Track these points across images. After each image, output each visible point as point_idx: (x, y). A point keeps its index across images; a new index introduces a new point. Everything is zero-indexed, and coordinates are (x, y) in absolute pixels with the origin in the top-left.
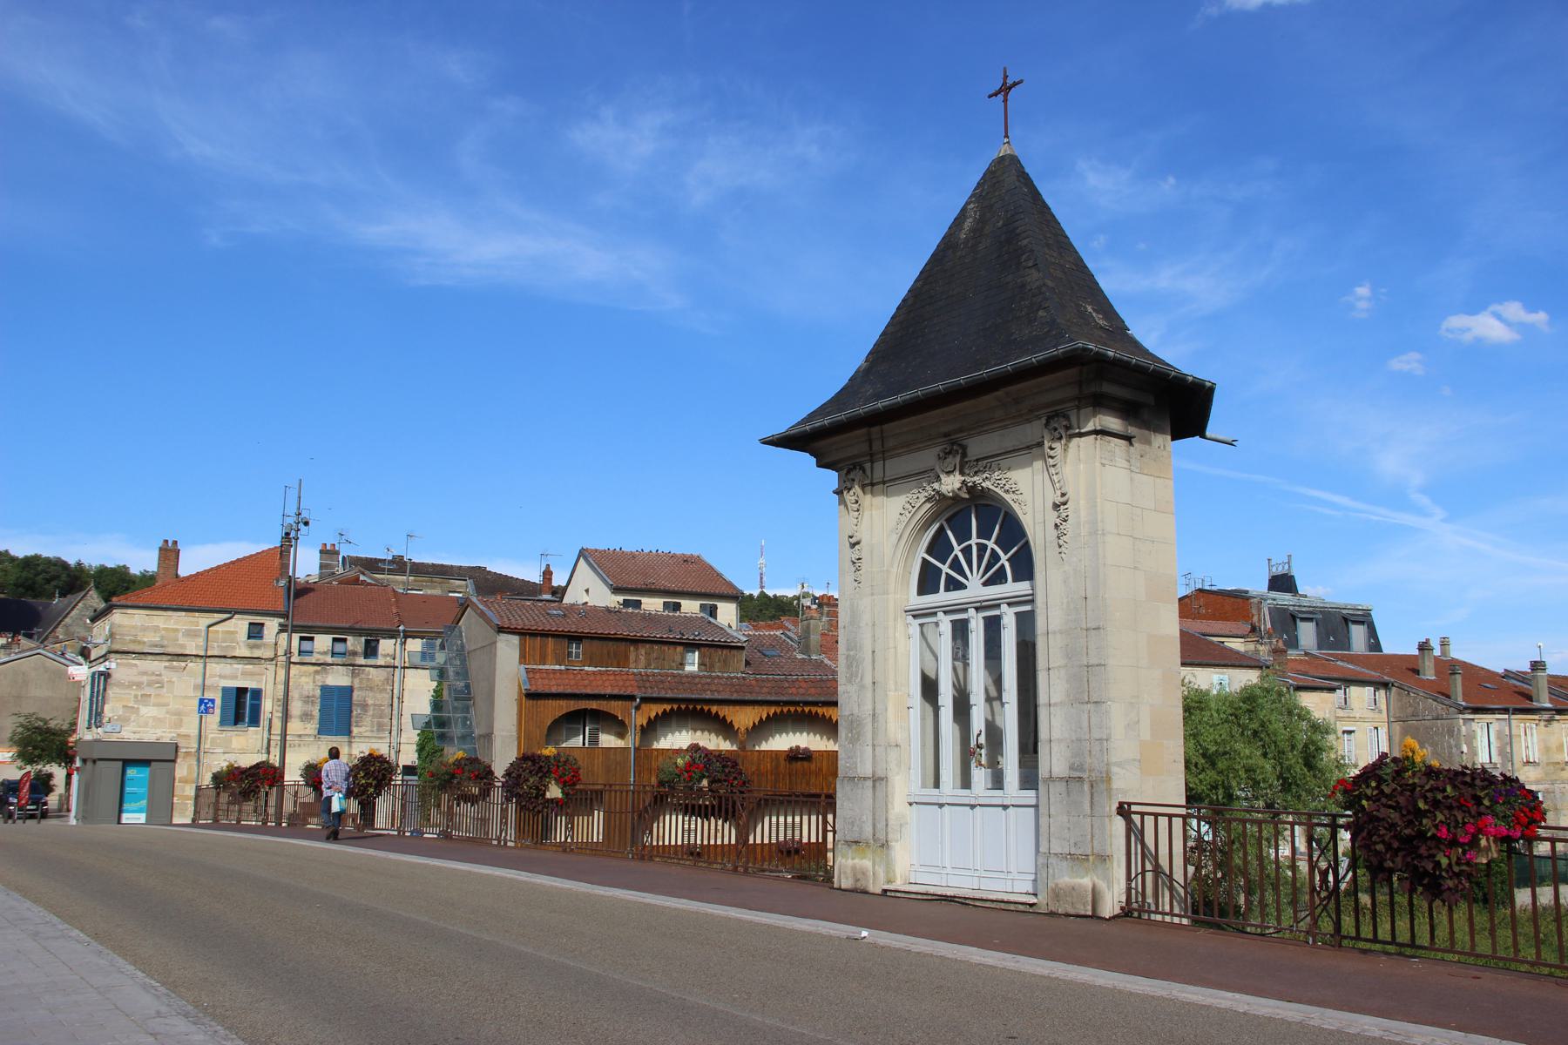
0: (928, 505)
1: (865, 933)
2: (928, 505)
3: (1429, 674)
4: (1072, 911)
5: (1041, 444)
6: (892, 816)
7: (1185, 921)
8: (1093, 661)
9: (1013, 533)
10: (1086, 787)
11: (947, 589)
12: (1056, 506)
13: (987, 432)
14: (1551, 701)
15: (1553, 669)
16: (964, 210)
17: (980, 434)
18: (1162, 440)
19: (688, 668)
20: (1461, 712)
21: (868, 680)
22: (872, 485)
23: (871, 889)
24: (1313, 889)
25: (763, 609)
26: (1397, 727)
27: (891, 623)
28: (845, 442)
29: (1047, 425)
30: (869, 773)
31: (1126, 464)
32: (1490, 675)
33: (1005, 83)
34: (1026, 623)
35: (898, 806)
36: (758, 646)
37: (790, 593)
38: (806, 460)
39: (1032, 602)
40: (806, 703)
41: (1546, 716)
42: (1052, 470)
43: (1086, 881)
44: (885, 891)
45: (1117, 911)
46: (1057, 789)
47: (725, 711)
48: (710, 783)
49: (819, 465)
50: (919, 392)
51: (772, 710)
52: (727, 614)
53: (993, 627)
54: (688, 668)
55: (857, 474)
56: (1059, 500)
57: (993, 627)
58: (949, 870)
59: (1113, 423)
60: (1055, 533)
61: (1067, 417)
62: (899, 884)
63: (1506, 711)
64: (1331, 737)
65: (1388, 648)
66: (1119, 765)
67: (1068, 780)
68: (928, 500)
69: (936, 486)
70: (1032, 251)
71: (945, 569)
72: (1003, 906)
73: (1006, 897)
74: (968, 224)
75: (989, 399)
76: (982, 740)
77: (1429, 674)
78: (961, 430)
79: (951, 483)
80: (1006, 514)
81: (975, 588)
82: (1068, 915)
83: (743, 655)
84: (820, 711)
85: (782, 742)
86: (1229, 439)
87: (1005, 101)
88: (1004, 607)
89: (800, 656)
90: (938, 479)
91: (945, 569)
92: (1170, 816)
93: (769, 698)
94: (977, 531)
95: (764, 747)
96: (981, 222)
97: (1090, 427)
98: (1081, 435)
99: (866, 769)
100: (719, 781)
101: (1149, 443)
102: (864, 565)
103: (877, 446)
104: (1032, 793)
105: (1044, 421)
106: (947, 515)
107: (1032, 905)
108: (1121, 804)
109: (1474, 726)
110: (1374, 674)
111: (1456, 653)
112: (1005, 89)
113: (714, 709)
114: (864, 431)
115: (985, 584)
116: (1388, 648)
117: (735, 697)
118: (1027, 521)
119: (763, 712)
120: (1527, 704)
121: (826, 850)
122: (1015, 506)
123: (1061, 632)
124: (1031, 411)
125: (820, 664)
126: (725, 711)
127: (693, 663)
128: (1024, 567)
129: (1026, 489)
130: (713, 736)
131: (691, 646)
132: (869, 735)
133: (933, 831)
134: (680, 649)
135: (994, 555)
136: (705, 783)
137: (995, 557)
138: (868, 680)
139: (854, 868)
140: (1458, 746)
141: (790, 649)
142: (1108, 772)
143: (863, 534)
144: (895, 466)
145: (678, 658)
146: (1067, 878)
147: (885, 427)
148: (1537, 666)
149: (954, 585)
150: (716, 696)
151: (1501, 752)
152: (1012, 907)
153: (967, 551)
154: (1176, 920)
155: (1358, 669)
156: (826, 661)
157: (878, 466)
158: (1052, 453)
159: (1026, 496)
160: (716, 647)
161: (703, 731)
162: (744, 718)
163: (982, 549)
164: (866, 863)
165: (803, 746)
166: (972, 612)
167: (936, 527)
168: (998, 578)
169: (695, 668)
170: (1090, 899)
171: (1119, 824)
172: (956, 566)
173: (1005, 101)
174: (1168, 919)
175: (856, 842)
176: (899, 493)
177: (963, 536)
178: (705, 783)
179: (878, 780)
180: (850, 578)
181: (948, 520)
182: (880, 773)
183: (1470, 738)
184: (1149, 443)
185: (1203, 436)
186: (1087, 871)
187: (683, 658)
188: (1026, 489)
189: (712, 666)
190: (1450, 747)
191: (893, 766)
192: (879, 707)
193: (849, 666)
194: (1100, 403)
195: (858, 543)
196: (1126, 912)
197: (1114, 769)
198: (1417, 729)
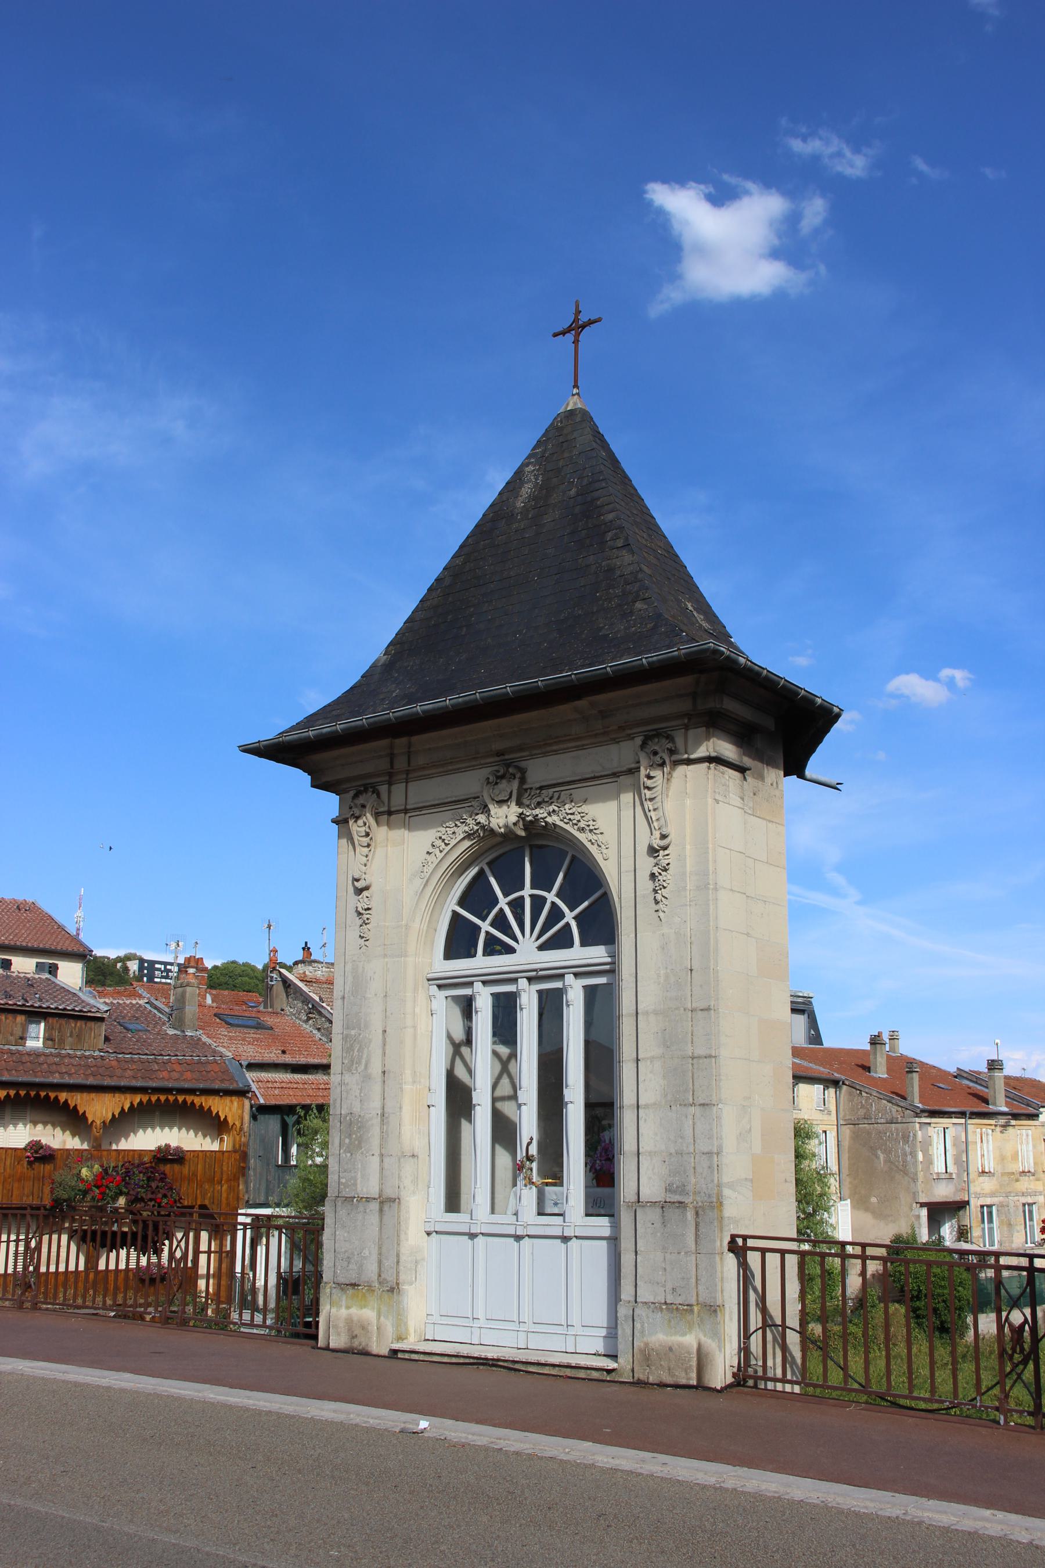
0: (467, 843)
1: (423, 1424)
2: (467, 843)
3: (881, 1072)
4: (669, 1380)
5: (634, 771)
6: (405, 1250)
7: (797, 1389)
8: (700, 1051)
9: (585, 882)
10: (690, 1215)
11: (489, 951)
12: (653, 851)
13: (556, 752)
14: (1007, 1104)
15: (1011, 1069)
16: (519, 474)
17: (545, 754)
18: (774, 775)
19: (31, 1044)
20: (917, 1115)
21: (376, 1069)
22: (390, 813)
23: (375, 1349)
24: (1002, 1352)
25: (102, 973)
26: (847, 1131)
27: (409, 994)
28: (354, 756)
29: (643, 746)
30: (374, 1192)
31: (737, 801)
32: (943, 1074)
33: (576, 320)
34: (601, 1003)
35: (413, 1236)
36: (117, 1016)
37: (113, 954)
38: (298, 778)
39: (612, 971)
40: (191, 1091)
41: (1002, 1121)
42: (649, 805)
43: (690, 1340)
44: (394, 1352)
45: (730, 1380)
46: (647, 1218)
47: (77, 1100)
48: (130, 1202)
49: (314, 785)
50: (477, 695)
51: (137, 1099)
52: (71, 974)
53: (551, 1006)
54: (31, 1044)
55: (368, 799)
56: (657, 843)
57: (551, 1006)
58: (482, 1323)
59: (727, 749)
60: (650, 885)
61: (670, 738)
62: (411, 1342)
63: (962, 1114)
64: (814, 1142)
65: (830, 1041)
66: (731, 1186)
67: (664, 1205)
68: (468, 836)
69: (482, 818)
70: (621, 528)
71: (485, 926)
72: (568, 1372)
73: (573, 1360)
74: (526, 490)
75: (564, 710)
76: (534, 1150)
77: (881, 1072)
78: (520, 749)
79: (504, 816)
80: (574, 857)
81: (527, 952)
82: (663, 1385)
83: (103, 1029)
84: (198, 1100)
85: (146, 1139)
86: (833, 781)
87: (576, 342)
88: (569, 979)
89: (171, 1032)
90: (485, 809)
91: (485, 926)
92: (783, 1252)
93: (134, 1083)
94: (533, 879)
95: (124, 1145)
96: (544, 491)
97: (701, 752)
98: (689, 762)
99: (370, 1186)
100: (142, 1200)
101: (761, 777)
102: (374, 917)
103: (401, 763)
104: (605, 1221)
105: (639, 741)
106: (487, 860)
107: (610, 1372)
108: (733, 1237)
109: (931, 1131)
110: (823, 1071)
111: (907, 1048)
112: (577, 328)
113: (63, 1096)
114: (384, 743)
115: (541, 948)
116: (830, 1041)
117: (91, 1081)
118: (609, 869)
119: (126, 1101)
120: (982, 1108)
121: (196, 1277)
122: (593, 849)
123: (656, 1013)
124: (621, 728)
125: (196, 1043)
126: (77, 1100)
127: (36, 1037)
128: (600, 925)
129: (608, 828)
130: (58, 1131)
131: (36, 1015)
132: (375, 1142)
133: (469, 1271)
134: (20, 1019)
135: (555, 909)
136: (122, 1201)
137: (556, 914)
138: (376, 1069)
139: (349, 1321)
140: (913, 1154)
141: (158, 1022)
142: (719, 1195)
143: (373, 877)
144: (422, 791)
145: (18, 1031)
146: (659, 1334)
147: (415, 739)
148: (994, 1065)
149: (494, 947)
150: (67, 1080)
151: (957, 1161)
152: (582, 1374)
153: (517, 906)
154: (788, 1388)
155: (805, 1063)
156: (204, 1039)
157: (398, 789)
158: (649, 783)
159: (609, 836)
160: (65, 1017)
161: (45, 1124)
162: (101, 1109)
163: (538, 902)
164: (368, 1314)
165: (174, 1144)
166: (523, 983)
167: (473, 872)
168: (562, 940)
169: (39, 1044)
170: (694, 1363)
171: (731, 1260)
172: (501, 922)
173: (576, 342)
174: (779, 1386)
175: (354, 1285)
176: (425, 827)
177: (513, 883)
178: (122, 1201)
179: (387, 1202)
180: (353, 933)
181: (489, 864)
182: (389, 1193)
183: (927, 1144)
184: (761, 777)
185: (801, 776)
186: (690, 1327)
187: (25, 1030)
188: (608, 828)
189: (62, 1041)
190: (905, 1154)
191: (407, 1182)
192: (389, 1104)
193: (348, 1049)
194: (715, 722)
195: (367, 888)
196: (742, 1379)
197: (726, 1192)
198: (869, 1133)
